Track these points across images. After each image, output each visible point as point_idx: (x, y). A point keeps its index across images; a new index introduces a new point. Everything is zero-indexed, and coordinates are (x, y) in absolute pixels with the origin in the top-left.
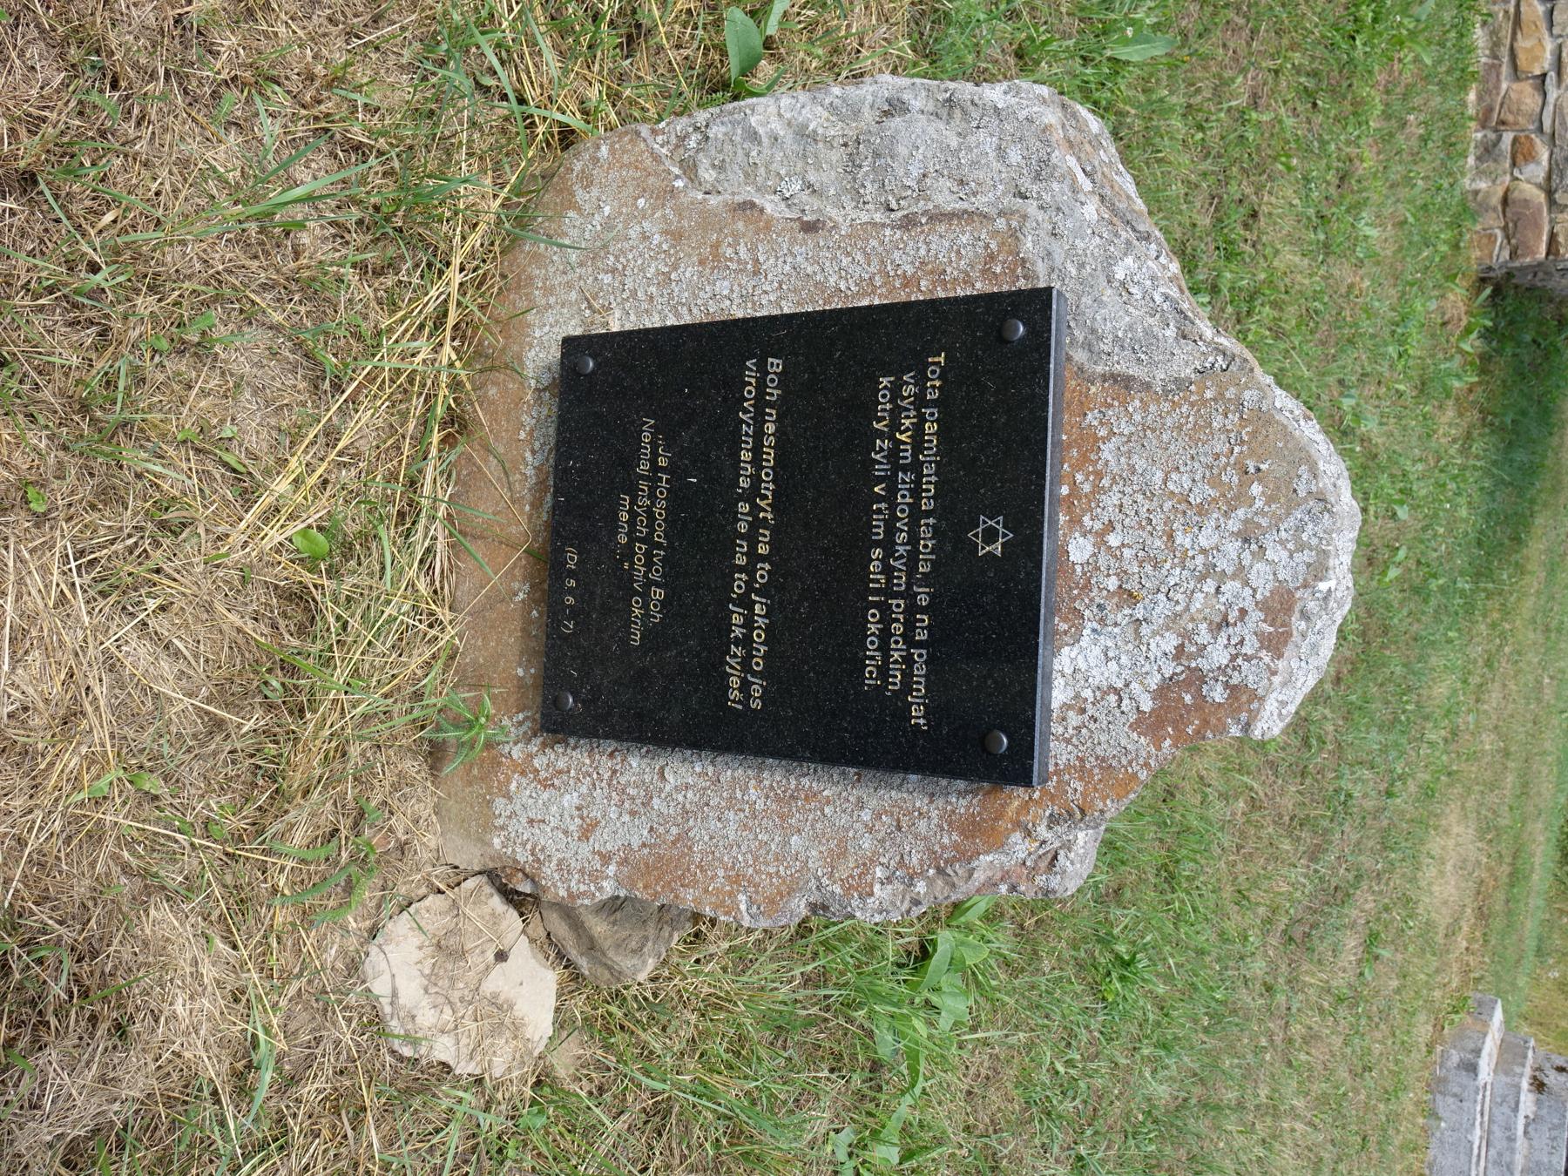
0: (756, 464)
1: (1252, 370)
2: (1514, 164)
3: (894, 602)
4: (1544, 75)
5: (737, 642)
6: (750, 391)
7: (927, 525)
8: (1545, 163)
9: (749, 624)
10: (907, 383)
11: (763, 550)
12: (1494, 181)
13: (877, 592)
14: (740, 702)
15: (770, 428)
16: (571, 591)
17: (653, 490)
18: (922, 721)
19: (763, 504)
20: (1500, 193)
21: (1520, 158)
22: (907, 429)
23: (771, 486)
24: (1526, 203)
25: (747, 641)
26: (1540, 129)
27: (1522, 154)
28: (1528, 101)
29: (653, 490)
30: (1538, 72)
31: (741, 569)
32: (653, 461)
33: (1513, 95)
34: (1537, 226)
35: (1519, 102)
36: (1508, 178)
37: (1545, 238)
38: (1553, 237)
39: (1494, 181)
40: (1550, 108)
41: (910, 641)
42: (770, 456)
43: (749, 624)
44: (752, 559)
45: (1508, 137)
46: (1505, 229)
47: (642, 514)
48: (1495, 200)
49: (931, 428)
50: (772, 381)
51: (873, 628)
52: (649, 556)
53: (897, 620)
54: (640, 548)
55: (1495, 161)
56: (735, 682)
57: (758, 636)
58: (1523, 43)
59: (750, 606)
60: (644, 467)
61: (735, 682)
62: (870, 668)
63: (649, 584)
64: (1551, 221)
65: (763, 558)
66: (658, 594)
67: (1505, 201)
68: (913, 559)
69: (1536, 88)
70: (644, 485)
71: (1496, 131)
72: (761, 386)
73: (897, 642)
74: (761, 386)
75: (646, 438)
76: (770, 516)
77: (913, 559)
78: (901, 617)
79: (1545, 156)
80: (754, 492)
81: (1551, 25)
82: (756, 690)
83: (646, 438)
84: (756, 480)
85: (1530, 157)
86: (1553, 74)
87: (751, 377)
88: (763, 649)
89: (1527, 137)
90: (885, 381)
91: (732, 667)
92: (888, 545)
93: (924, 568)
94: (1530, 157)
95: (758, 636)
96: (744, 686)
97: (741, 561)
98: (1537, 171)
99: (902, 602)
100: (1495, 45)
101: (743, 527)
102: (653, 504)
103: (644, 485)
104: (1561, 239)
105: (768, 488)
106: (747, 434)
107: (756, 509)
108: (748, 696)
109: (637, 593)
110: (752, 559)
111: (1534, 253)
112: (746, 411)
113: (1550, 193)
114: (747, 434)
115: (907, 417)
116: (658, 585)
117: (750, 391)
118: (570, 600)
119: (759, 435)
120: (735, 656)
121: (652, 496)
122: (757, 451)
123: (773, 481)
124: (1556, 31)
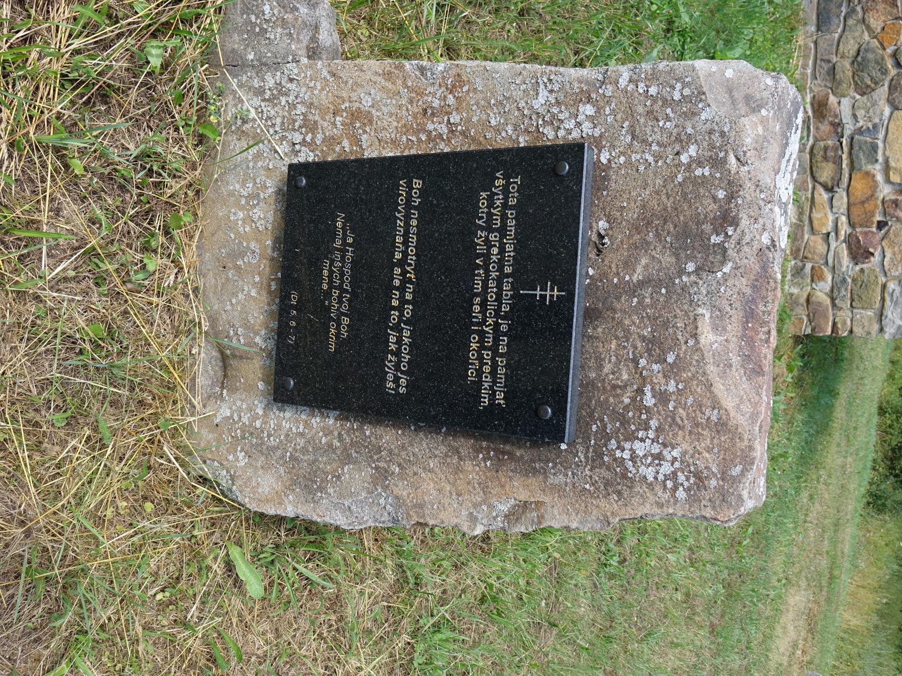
1: (641, 525)
2: (812, 281)
3: (486, 353)
4: (828, 234)
6: (402, 200)
7: (508, 282)
8: (830, 282)
9: (399, 342)
10: (499, 178)
11: (409, 297)
12: (802, 289)
13: (478, 324)
14: (393, 389)
15: (414, 223)
17: (343, 257)
18: (502, 402)
19: (408, 269)
20: (805, 296)
21: (815, 278)
22: (498, 207)
23: (414, 258)
25: (397, 353)
26: (827, 263)
27: (816, 276)
28: (820, 247)
29: (343, 257)
30: (825, 232)
31: (394, 308)
32: (344, 239)
34: (826, 317)
35: (814, 247)
36: (809, 288)
37: (830, 324)
38: (834, 324)
39: (802, 289)
40: (831, 253)
41: (495, 353)
43: (399, 342)
44: (401, 306)
45: (809, 266)
46: (808, 316)
47: (337, 271)
48: (803, 300)
52: (340, 297)
53: (487, 364)
54: (336, 293)
55: (802, 278)
56: (390, 377)
57: (405, 350)
58: (816, 215)
59: (400, 331)
60: (338, 243)
64: (833, 315)
65: (408, 302)
66: (346, 321)
67: (808, 301)
69: (823, 240)
70: (338, 254)
71: (802, 261)
73: (486, 377)
75: (339, 224)
79: (830, 278)
80: (402, 263)
81: (832, 207)
83: (339, 224)
84: (405, 254)
85: (821, 278)
86: (833, 234)
88: (408, 357)
89: (819, 267)
94: (821, 278)
95: (405, 350)
96: (396, 382)
98: (826, 285)
99: (490, 353)
100: (801, 214)
101: (397, 283)
102: (343, 266)
104: (839, 326)
107: (404, 273)
108: (398, 386)
110: (401, 306)
111: (825, 332)
112: (399, 212)
113: (833, 300)
114: (400, 226)
115: (499, 199)
116: (346, 315)
117: (402, 200)
119: (407, 226)
120: (391, 361)
124: (834, 210)
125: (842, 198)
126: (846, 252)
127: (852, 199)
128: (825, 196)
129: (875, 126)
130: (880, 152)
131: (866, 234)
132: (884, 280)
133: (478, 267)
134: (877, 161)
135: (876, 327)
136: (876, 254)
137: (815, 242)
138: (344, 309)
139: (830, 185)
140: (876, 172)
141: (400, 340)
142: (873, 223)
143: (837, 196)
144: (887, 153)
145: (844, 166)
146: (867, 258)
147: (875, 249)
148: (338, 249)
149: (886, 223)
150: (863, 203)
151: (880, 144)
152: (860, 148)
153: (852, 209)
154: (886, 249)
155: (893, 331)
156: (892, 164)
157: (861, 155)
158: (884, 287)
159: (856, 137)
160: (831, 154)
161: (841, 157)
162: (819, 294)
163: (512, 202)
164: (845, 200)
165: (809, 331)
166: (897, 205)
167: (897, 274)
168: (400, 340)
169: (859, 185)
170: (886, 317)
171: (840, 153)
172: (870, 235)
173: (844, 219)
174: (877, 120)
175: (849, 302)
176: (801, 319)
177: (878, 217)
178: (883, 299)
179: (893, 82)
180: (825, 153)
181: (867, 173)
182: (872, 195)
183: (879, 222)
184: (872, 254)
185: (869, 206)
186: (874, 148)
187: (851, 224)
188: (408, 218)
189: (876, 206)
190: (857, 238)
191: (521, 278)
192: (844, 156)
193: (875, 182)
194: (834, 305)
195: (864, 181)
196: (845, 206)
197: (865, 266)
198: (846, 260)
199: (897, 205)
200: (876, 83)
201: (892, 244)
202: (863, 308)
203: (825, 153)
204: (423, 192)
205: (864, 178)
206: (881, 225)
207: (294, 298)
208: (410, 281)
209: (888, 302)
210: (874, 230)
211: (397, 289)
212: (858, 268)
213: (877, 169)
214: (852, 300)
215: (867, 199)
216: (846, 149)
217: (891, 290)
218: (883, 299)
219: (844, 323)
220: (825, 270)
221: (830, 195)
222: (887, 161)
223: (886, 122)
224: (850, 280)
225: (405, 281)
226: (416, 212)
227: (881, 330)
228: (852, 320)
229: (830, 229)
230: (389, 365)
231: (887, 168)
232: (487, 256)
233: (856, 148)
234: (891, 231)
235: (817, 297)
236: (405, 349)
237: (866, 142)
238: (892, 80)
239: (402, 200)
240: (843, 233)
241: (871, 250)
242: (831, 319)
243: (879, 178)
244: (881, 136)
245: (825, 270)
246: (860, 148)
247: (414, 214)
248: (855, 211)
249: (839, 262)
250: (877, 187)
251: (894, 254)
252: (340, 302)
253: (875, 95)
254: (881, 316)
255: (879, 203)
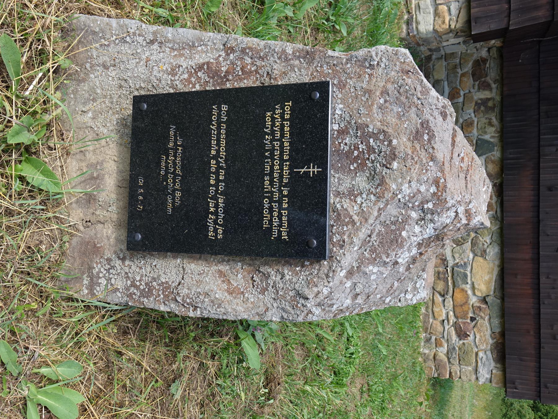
0: (218, 146)
2: (436, 346)
5: (212, 213)
7: (286, 165)
9: (216, 206)
10: (278, 109)
12: (430, 351)
14: (213, 236)
16: (141, 194)
18: (286, 237)
21: (438, 345)
23: (224, 154)
24: (441, 361)
25: (216, 213)
26: (444, 337)
27: (438, 344)
28: (439, 328)
31: (212, 186)
32: (175, 142)
33: (434, 325)
34: (445, 369)
38: (450, 373)
39: (430, 351)
42: (223, 143)
43: (216, 206)
44: (217, 181)
45: (433, 338)
46: (435, 366)
47: (172, 162)
48: (431, 357)
49: (287, 129)
50: (224, 113)
51: (266, 206)
52: (174, 179)
56: (211, 229)
58: (436, 309)
59: (216, 199)
60: (171, 145)
61: (211, 229)
62: (266, 220)
63: (174, 191)
64: (450, 367)
66: (178, 194)
67: (434, 358)
68: (281, 176)
69: (441, 323)
72: (219, 115)
73: (275, 219)
74: (219, 115)
75: (172, 133)
76: (224, 165)
77: (281, 176)
78: (277, 210)
80: (216, 157)
81: (444, 306)
82: (220, 231)
83: (172, 133)
84: (218, 151)
85: (441, 345)
86: (446, 321)
87: (215, 112)
88: (222, 215)
90: (269, 114)
91: (209, 223)
92: (271, 174)
93: (285, 181)
96: (215, 230)
97: (212, 182)
102: (176, 159)
103: (171, 152)
104: (453, 374)
105: (223, 154)
106: (214, 134)
107: (218, 163)
108: (217, 234)
109: (169, 194)
110: (217, 181)
113: (449, 359)
114: (214, 134)
115: (278, 121)
118: (141, 198)
119: (219, 134)
120: (211, 219)
121: (175, 156)
122: (218, 140)
123: (225, 152)
124: (446, 308)
125: (450, 302)
126: (454, 332)
127: (455, 303)
128: (441, 299)
129: (465, 264)
130: (469, 278)
131: (464, 323)
132: (477, 350)
133: (267, 157)
134: (467, 283)
135: (474, 377)
136: (471, 335)
137: (437, 325)
138: (177, 187)
139: (442, 293)
140: (467, 289)
141: (217, 205)
142: (468, 318)
143: (446, 301)
144: (473, 279)
145: (450, 284)
146: (466, 337)
147: (470, 333)
148: (171, 149)
149: (475, 319)
150: (461, 306)
151: (469, 274)
152: (458, 275)
153: (456, 309)
154: (476, 333)
155: (483, 380)
156: (476, 286)
157: (459, 279)
158: (477, 354)
159: (455, 268)
160: (442, 276)
161: (447, 278)
162: (440, 354)
163: (287, 117)
164: (452, 303)
165: (436, 375)
166: (480, 310)
167: (483, 348)
168: (217, 205)
169: (458, 295)
170: (479, 372)
171: (447, 276)
172: (467, 324)
173: (451, 313)
174: (466, 260)
175: (458, 361)
176: (431, 368)
177: (471, 315)
178: (477, 361)
179: (474, 241)
180: (439, 275)
181: (463, 290)
182: (466, 302)
183: (471, 317)
184: (469, 336)
185: (465, 308)
186: (466, 276)
187: (455, 316)
188: (219, 128)
189: (469, 308)
190: (460, 325)
191: (294, 163)
192: (449, 278)
193: (467, 295)
194: (449, 362)
195: (461, 294)
196: (452, 306)
197: (465, 341)
198: (454, 337)
199: (480, 310)
200: (464, 240)
201: (479, 331)
202: (466, 365)
203: (439, 275)
204: (228, 113)
205: (461, 292)
206: (472, 319)
207: (141, 181)
208: (222, 168)
209: (479, 364)
210: (469, 321)
211: (213, 173)
212: (461, 342)
213: (468, 287)
214: (460, 360)
215: (464, 304)
216: (450, 274)
217: (481, 357)
218: (477, 361)
219: (456, 373)
220: (443, 341)
221: (443, 298)
222: (473, 284)
223: (471, 261)
224: (457, 349)
225: (219, 168)
226: (225, 125)
227: (477, 378)
228: (460, 371)
229: (444, 318)
230: (210, 221)
231: (473, 288)
232: (272, 151)
233: (456, 275)
234: (478, 324)
235: (439, 356)
236: (221, 210)
237: (461, 272)
238: (472, 239)
239: (215, 118)
240: (451, 321)
241: (468, 333)
242: (448, 369)
243: (470, 292)
244: (469, 269)
245: (443, 341)
246: (458, 275)
247: (223, 126)
248: (458, 310)
249: (451, 338)
250: (469, 298)
251: (481, 337)
252: (174, 182)
253: (464, 246)
254: (476, 370)
255: (471, 306)
